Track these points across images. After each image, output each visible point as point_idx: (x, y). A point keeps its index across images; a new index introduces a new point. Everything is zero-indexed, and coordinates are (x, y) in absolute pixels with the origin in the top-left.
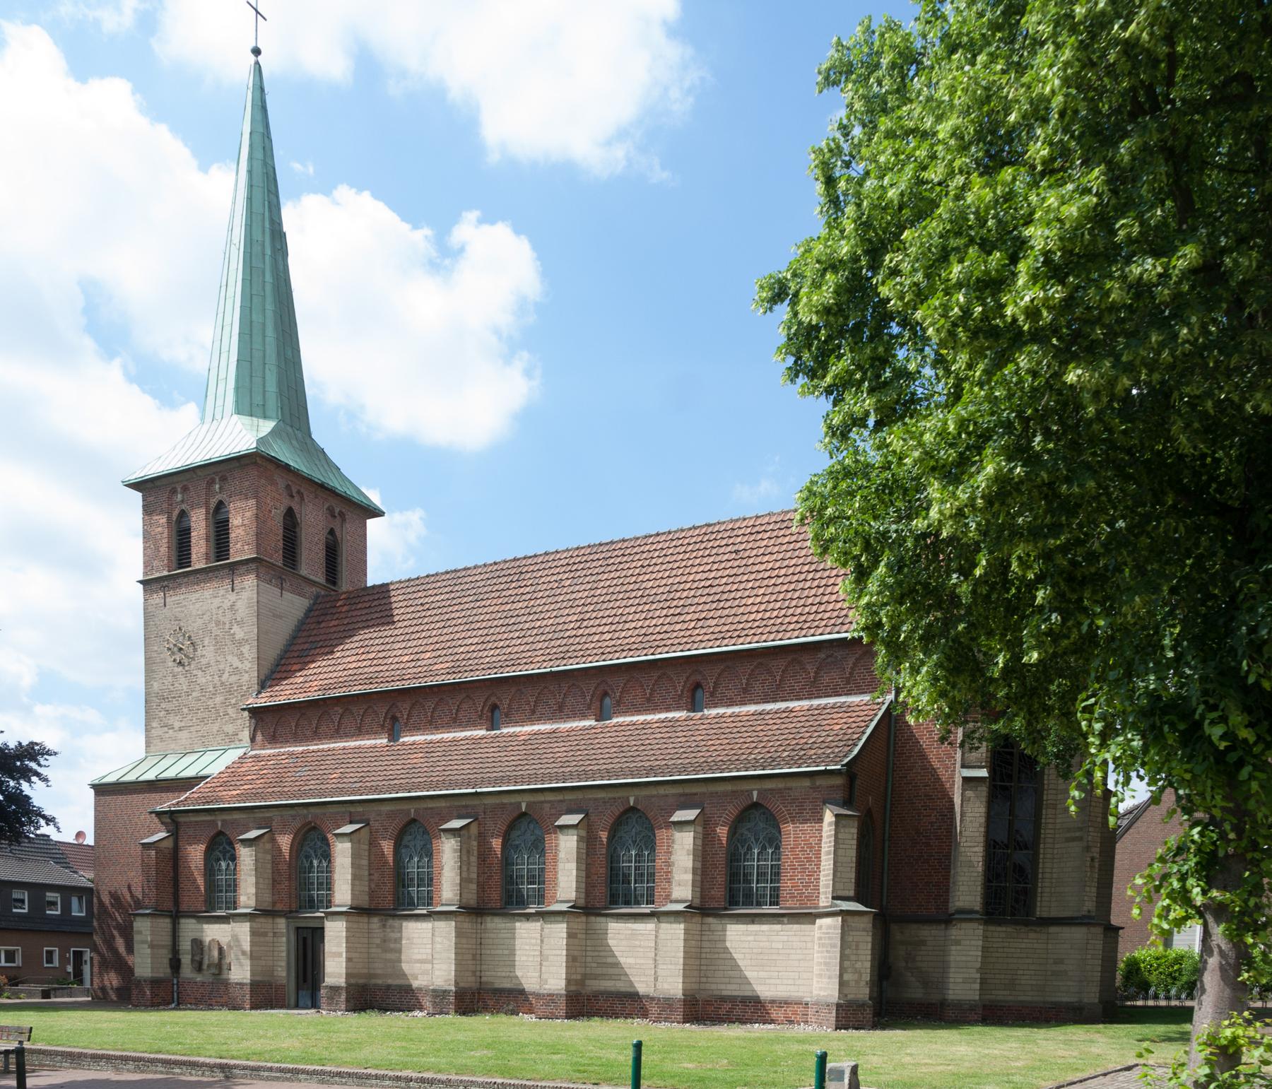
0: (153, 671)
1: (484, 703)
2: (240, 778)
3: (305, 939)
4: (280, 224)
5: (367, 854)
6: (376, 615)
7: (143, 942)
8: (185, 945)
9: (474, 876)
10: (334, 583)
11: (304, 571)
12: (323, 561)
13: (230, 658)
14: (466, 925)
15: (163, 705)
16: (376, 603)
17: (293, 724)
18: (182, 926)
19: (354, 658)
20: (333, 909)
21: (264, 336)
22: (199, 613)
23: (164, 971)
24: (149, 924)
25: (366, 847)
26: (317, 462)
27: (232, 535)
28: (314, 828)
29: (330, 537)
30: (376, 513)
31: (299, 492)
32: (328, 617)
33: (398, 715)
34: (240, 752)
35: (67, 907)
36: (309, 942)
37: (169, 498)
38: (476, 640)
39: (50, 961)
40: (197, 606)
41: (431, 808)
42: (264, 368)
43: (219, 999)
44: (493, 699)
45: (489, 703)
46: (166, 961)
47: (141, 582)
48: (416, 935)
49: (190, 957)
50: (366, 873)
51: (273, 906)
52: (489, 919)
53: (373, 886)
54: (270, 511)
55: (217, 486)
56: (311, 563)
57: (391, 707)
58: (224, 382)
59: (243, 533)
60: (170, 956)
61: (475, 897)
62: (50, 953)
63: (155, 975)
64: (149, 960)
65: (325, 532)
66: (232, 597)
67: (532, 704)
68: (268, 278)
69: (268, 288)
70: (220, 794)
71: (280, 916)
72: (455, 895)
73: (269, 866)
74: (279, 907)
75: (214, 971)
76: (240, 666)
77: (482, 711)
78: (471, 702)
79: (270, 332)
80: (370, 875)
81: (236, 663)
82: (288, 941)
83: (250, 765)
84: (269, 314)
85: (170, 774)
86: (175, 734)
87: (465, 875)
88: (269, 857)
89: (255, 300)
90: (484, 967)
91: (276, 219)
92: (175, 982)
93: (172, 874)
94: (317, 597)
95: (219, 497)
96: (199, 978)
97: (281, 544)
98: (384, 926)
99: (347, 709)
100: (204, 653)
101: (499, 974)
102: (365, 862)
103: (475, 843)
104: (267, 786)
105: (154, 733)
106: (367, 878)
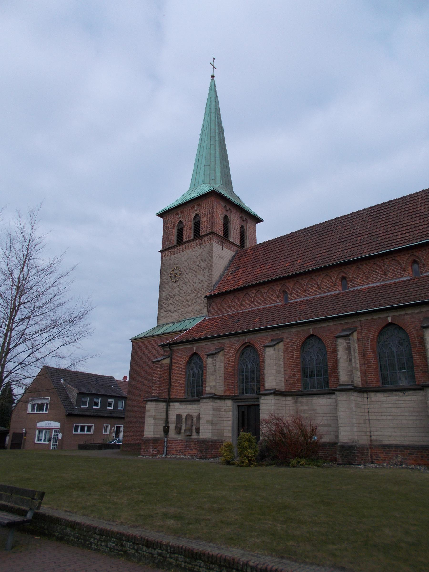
0: (163, 288)
3: (243, 412)
4: (221, 124)
5: (282, 357)
7: (150, 416)
8: (172, 418)
9: (358, 366)
10: (243, 247)
11: (232, 240)
12: (239, 237)
15: (167, 302)
17: (230, 302)
21: (215, 157)
22: (185, 260)
23: (160, 434)
24: (154, 406)
25: (282, 354)
27: (202, 226)
28: (248, 346)
29: (242, 229)
30: (259, 220)
33: (287, 290)
34: (203, 318)
35: (116, 406)
36: (246, 413)
38: (324, 251)
39: (106, 431)
41: (323, 327)
42: (215, 167)
43: (190, 451)
46: (162, 428)
47: (160, 251)
49: (175, 425)
50: (283, 370)
51: (225, 393)
53: (287, 377)
56: (235, 237)
58: (197, 183)
60: (164, 425)
64: (153, 427)
66: (200, 250)
68: (217, 139)
69: (217, 142)
70: (194, 335)
73: (223, 369)
78: (329, 278)
79: (218, 155)
80: (285, 371)
81: (201, 278)
86: (171, 314)
89: (212, 146)
90: (372, 429)
92: (166, 440)
93: (168, 378)
94: (237, 251)
96: (180, 438)
97: (222, 228)
98: (296, 402)
101: (386, 434)
102: (282, 363)
103: (356, 345)
105: (162, 314)
106: (283, 373)
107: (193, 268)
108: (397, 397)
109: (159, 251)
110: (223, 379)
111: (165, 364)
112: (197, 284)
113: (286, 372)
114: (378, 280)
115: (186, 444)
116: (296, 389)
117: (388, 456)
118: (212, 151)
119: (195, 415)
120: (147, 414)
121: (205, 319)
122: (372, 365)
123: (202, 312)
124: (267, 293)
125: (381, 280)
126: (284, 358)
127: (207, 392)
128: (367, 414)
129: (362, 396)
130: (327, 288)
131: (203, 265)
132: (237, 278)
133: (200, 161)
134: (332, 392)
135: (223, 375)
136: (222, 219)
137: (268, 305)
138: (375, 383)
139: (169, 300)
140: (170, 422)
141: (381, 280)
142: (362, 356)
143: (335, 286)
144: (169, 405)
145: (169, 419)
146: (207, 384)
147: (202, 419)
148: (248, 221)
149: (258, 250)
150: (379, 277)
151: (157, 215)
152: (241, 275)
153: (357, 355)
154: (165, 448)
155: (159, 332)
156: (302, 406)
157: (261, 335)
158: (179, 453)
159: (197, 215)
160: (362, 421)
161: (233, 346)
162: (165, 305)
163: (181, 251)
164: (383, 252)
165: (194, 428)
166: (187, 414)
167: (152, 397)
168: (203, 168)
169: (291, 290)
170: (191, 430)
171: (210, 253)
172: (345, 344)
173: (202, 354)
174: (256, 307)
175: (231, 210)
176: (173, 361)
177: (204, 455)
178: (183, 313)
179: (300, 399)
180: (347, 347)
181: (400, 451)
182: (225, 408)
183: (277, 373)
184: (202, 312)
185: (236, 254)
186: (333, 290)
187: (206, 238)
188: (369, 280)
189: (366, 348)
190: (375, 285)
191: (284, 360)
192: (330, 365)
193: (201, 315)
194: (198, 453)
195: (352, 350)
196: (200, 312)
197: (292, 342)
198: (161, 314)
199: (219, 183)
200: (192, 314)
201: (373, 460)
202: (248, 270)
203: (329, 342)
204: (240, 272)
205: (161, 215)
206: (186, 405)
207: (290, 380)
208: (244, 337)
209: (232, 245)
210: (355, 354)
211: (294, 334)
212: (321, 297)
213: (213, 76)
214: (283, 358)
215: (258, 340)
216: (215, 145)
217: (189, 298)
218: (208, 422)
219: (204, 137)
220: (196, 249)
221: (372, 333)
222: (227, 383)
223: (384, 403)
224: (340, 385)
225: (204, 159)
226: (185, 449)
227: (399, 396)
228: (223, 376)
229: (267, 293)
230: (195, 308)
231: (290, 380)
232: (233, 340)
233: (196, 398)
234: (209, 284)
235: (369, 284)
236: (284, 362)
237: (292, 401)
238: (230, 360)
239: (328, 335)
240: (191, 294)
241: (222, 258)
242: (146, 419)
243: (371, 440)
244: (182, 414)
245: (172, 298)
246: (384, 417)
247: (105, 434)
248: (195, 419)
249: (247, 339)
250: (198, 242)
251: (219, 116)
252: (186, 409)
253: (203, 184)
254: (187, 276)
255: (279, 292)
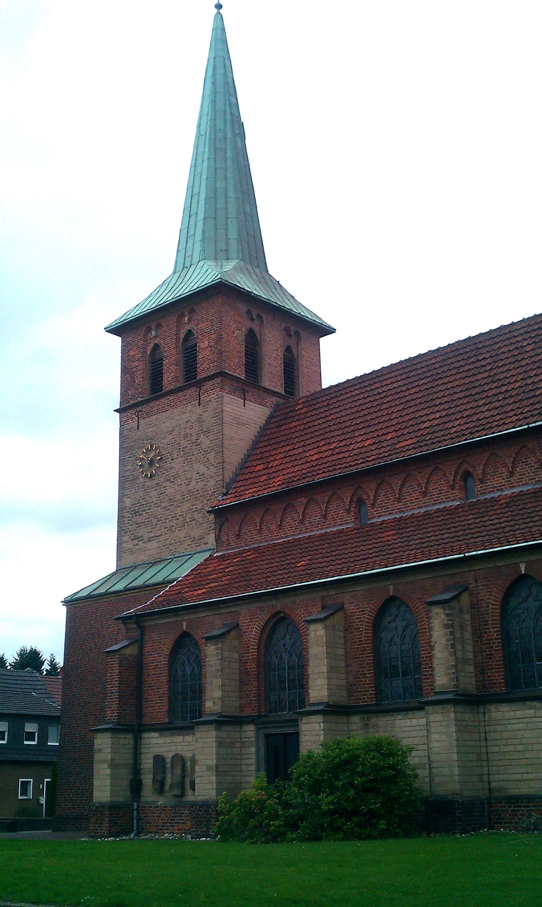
1: (456, 472)
2: (206, 578)
5: (342, 641)
6: (335, 410)
7: (103, 761)
8: (147, 763)
9: (471, 656)
10: (292, 394)
11: (266, 383)
13: (196, 466)
14: (468, 716)
16: (334, 400)
17: (258, 521)
18: (144, 741)
19: (315, 451)
20: (307, 709)
23: (123, 796)
24: (109, 741)
26: (274, 291)
27: (200, 356)
28: (284, 618)
30: (328, 331)
31: (259, 316)
32: (289, 420)
34: (207, 555)
37: (145, 336)
38: (438, 415)
39: (24, 793)
40: (167, 424)
41: (411, 583)
42: (227, 221)
44: (465, 467)
45: (462, 469)
46: (126, 782)
48: (405, 735)
50: (343, 664)
52: (492, 708)
53: (351, 679)
54: (234, 332)
55: (186, 318)
57: (356, 491)
58: (194, 216)
59: (209, 353)
60: (131, 777)
61: (473, 681)
62: (25, 785)
63: (115, 799)
64: (108, 782)
65: (282, 349)
66: (199, 410)
67: (510, 465)
68: (229, 154)
71: (249, 723)
72: (451, 679)
73: (236, 666)
74: (247, 712)
75: (177, 792)
76: (206, 472)
77: (454, 480)
82: (258, 751)
83: (215, 565)
84: (230, 181)
85: (139, 582)
87: (459, 655)
88: (236, 656)
89: (219, 172)
91: (236, 113)
92: (135, 807)
94: (277, 406)
95: (188, 327)
98: (366, 726)
99: (311, 499)
100: (173, 465)
101: (513, 777)
102: (341, 651)
103: (467, 617)
104: (232, 581)
106: (343, 670)
107: (186, 447)
108: (532, 711)
109: (115, 411)
110: (238, 684)
111: (130, 655)
112: (194, 483)
113: (350, 669)
114: (531, 480)
115: (174, 813)
116: (367, 702)
117: (517, 815)
118: (218, 184)
119: (188, 755)
120: (97, 757)
121: (211, 555)
122: (493, 654)
123: (205, 540)
124: (328, 503)
125: (535, 479)
126: (345, 644)
127: (208, 711)
128: (483, 743)
129: (476, 711)
130: (438, 494)
131: (206, 442)
132: (273, 469)
133: (194, 206)
134: (420, 707)
135: (237, 677)
136: (242, 338)
137: (330, 527)
138: (498, 687)
139: (140, 515)
140: (143, 771)
141: (535, 479)
142: (477, 638)
143: (453, 490)
144: (139, 737)
145: (140, 764)
146: (207, 696)
147: (199, 763)
148: (302, 335)
149: (317, 406)
150: (533, 472)
151: (107, 331)
152: (281, 461)
153: (468, 635)
154: (135, 821)
155: (120, 586)
156: (377, 732)
157: (306, 597)
158: (162, 829)
159: (190, 332)
160: (474, 757)
161: (254, 618)
162: (131, 525)
163: (159, 411)
164: (537, 424)
165: (187, 781)
166: (173, 754)
167: (105, 723)
168: (200, 225)
169: (372, 498)
170: (182, 786)
171: (219, 414)
172: (443, 617)
173: (199, 634)
174: (307, 532)
175: (261, 317)
176: (146, 650)
177: (205, 831)
178: (168, 542)
179: (374, 720)
180: (446, 622)
181: (534, 806)
182: (243, 740)
183: (330, 672)
184: (205, 540)
185: (274, 412)
186: (449, 498)
187: (208, 385)
188: (515, 480)
189: (484, 621)
190: (525, 489)
191: (345, 646)
192: (425, 654)
193: (204, 547)
194: (192, 828)
195: (457, 627)
196: (202, 541)
197: (360, 612)
198: (124, 545)
199: (236, 256)
200: (185, 545)
201: (492, 824)
202: (295, 452)
203: (422, 611)
204: (280, 456)
205: (115, 330)
206: (171, 736)
207: (356, 685)
208: (274, 602)
209: (265, 395)
210: (462, 634)
211: (362, 595)
212: (426, 514)
213: (219, 6)
214: (343, 642)
215: (298, 608)
216: (226, 169)
217: (178, 511)
218: (209, 768)
219: (201, 150)
220: (189, 408)
221: (494, 594)
222: (246, 691)
223: (513, 722)
224: (436, 693)
225: (202, 203)
226: (173, 823)
227: (535, 708)
228: (238, 678)
229: (328, 503)
230: (192, 534)
231: (356, 685)
232: (254, 606)
233: (187, 723)
234: (217, 482)
235: (515, 486)
236: (345, 649)
237: (359, 725)
238: (249, 647)
239: (421, 598)
240: (182, 502)
241: (243, 424)
242: (96, 766)
243: (490, 790)
244: (165, 755)
245: (145, 510)
246: (511, 748)
247: (22, 799)
248: (189, 763)
249: (279, 606)
250: (193, 391)
251: (233, 99)
252: (172, 744)
253: (201, 263)
254: (173, 465)
255: (351, 501)
